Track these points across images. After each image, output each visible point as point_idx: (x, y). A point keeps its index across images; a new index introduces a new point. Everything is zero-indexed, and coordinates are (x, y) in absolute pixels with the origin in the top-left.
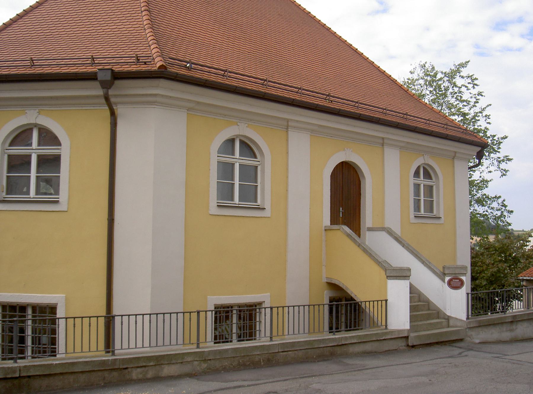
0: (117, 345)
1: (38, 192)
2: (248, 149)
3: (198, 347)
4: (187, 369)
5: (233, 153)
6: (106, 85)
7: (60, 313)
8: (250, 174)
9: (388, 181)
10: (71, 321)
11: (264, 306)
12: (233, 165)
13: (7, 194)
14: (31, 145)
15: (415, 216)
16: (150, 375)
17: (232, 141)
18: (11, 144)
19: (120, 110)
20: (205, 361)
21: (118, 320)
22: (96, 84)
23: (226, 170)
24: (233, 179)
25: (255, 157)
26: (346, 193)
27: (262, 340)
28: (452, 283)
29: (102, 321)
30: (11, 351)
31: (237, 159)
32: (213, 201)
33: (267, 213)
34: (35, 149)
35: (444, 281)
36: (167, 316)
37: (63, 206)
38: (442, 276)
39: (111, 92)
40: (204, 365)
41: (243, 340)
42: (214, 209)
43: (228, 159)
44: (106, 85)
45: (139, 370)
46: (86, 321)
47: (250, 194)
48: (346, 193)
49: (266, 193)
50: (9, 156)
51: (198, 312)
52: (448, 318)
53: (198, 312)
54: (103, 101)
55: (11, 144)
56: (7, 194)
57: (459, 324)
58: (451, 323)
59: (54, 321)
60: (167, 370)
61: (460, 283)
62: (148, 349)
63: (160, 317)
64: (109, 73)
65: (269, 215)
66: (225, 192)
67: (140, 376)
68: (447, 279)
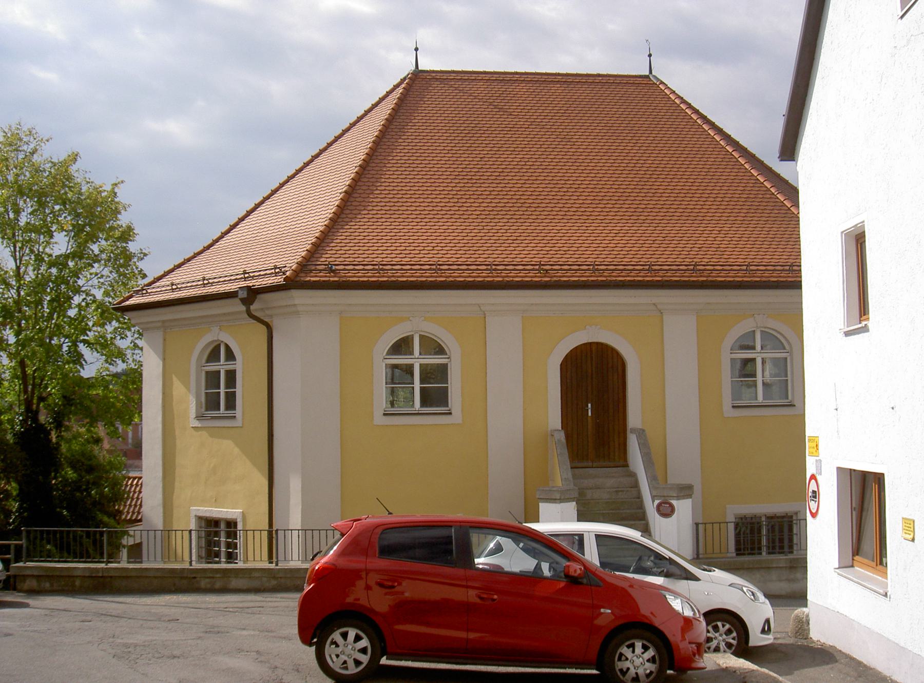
3: (277, 565)
4: (256, 584)
7: (240, 527)
14: (412, 353)
15: (733, 407)
16: (218, 585)
18: (208, 361)
20: (274, 578)
27: (240, 565)
29: (265, 535)
30: (740, 550)
33: (238, 423)
34: (417, 360)
35: (653, 502)
39: (252, 307)
40: (274, 582)
41: (744, 554)
43: (212, 367)
45: (207, 580)
50: (207, 373)
53: (190, 531)
55: (208, 361)
60: (235, 583)
61: (670, 509)
65: (460, 421)
67: (209, 586)
68: (657, 502)
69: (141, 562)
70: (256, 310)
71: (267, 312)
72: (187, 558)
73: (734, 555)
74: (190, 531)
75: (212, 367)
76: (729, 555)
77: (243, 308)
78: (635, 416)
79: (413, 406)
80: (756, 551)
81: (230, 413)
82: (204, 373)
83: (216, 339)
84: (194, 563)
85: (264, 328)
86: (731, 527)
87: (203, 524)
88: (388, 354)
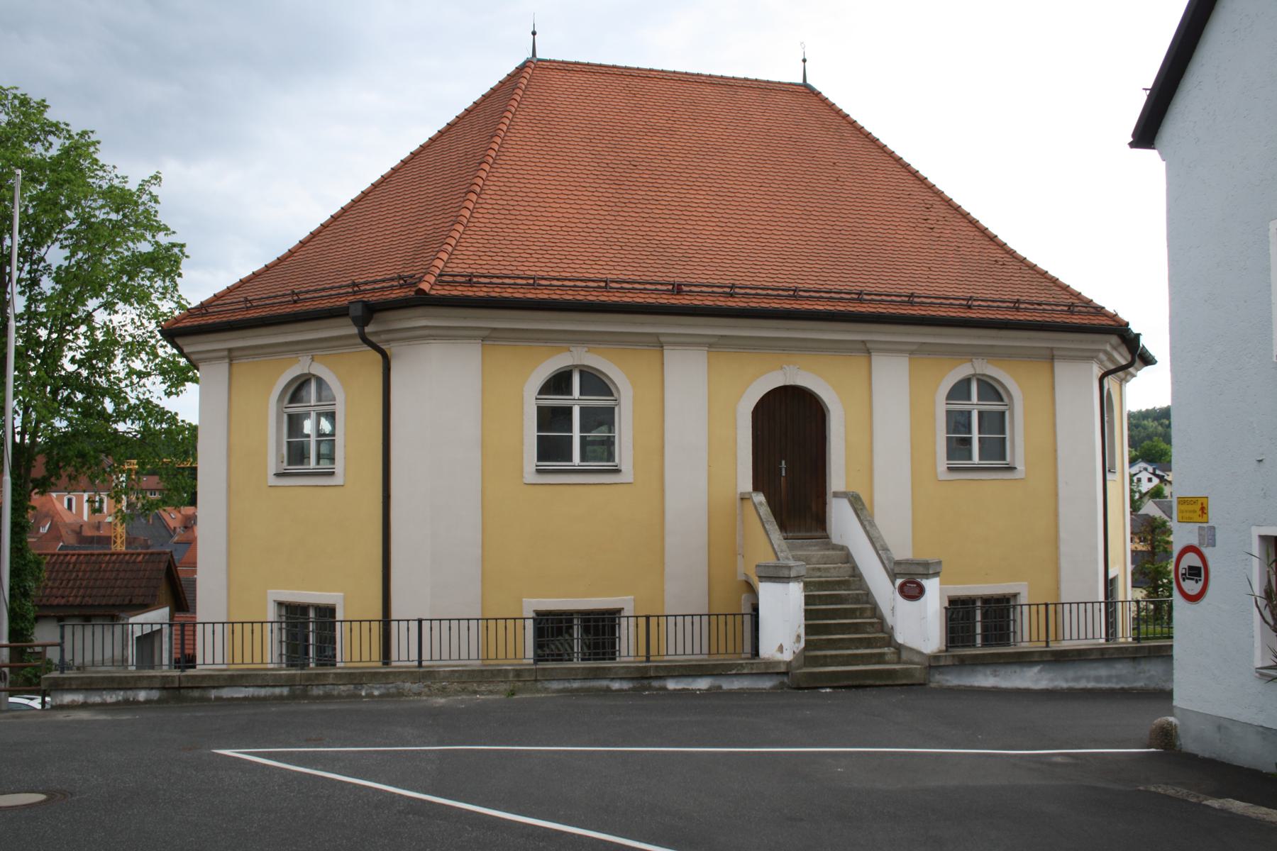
0: (394, 655)
1: (583, 458)
2: (991, 390)
5: (969, 398)
6: (362, 322)
7: (339, 615)
8: (995, 423)
9: (884, 420)
10: (1034, 608)
11: (625, 613)
12: (969, 413)
13: (289, 464)
17: (966, 382)
19: (393, 349)
21: (394, 625)
22: (348, 321)
23: (958, 422)
24: (970, 431)
25: (1001, 399)
26: (791, 446)
28: (906, 589)
31: (975, 405)
32: (942, 462)
33: (338, 480)
36: (257, 627)
37: (627, 475)
38: (893, 576)
39: (368, 329)
42: (530, 475)
43: (959, 406)
44: (362, 322)
46: (1082, 606)
47: (996, 449)
48: (791, 446)
49: (625, 453)
51: (648, 618)
52: (899, 648)
53: (420, 621)
54: (359, 341)
56: (289, 464)
57: (916, 659)
58: (904, 656)
59: (333, 624)
62: (726, 657)
63: (248, 627)
64: (360, 306)
65: (631, 480)
66: (958, 447)
68: (899, 582)
69: (1008, 645)
70: (376, 333)
71: (383, 337)
72: (1043, 637)
73: (380, 664)
74: (1047, 605)
75: (959, 406)
76: (525, 661)
77: (355, 330)
78: (837, 479)
79: (970, 458)
80: (566, 657)
81: (325, 465)
82: (285, 417)
83: (306, 371)
84: (1051, 644)
85: (379, 357)
86: (530, 624)
87: (284, 612)
88: (540, 393)
